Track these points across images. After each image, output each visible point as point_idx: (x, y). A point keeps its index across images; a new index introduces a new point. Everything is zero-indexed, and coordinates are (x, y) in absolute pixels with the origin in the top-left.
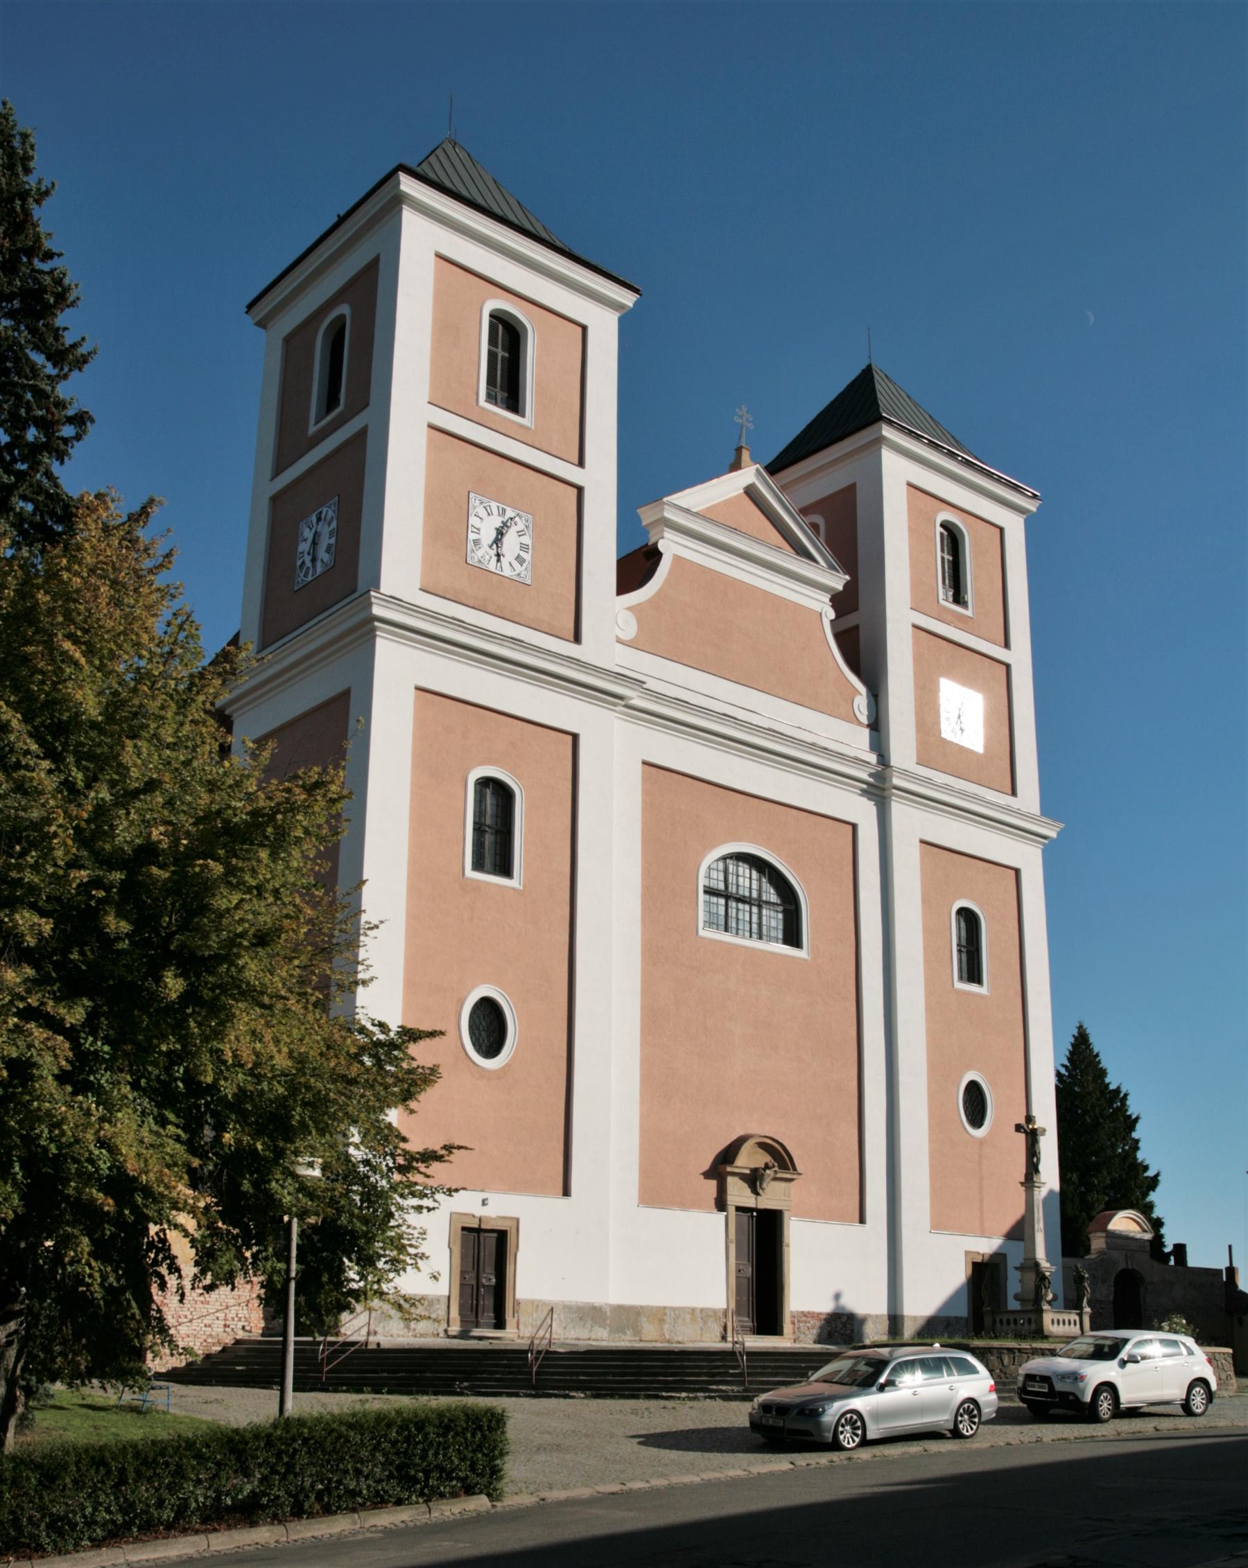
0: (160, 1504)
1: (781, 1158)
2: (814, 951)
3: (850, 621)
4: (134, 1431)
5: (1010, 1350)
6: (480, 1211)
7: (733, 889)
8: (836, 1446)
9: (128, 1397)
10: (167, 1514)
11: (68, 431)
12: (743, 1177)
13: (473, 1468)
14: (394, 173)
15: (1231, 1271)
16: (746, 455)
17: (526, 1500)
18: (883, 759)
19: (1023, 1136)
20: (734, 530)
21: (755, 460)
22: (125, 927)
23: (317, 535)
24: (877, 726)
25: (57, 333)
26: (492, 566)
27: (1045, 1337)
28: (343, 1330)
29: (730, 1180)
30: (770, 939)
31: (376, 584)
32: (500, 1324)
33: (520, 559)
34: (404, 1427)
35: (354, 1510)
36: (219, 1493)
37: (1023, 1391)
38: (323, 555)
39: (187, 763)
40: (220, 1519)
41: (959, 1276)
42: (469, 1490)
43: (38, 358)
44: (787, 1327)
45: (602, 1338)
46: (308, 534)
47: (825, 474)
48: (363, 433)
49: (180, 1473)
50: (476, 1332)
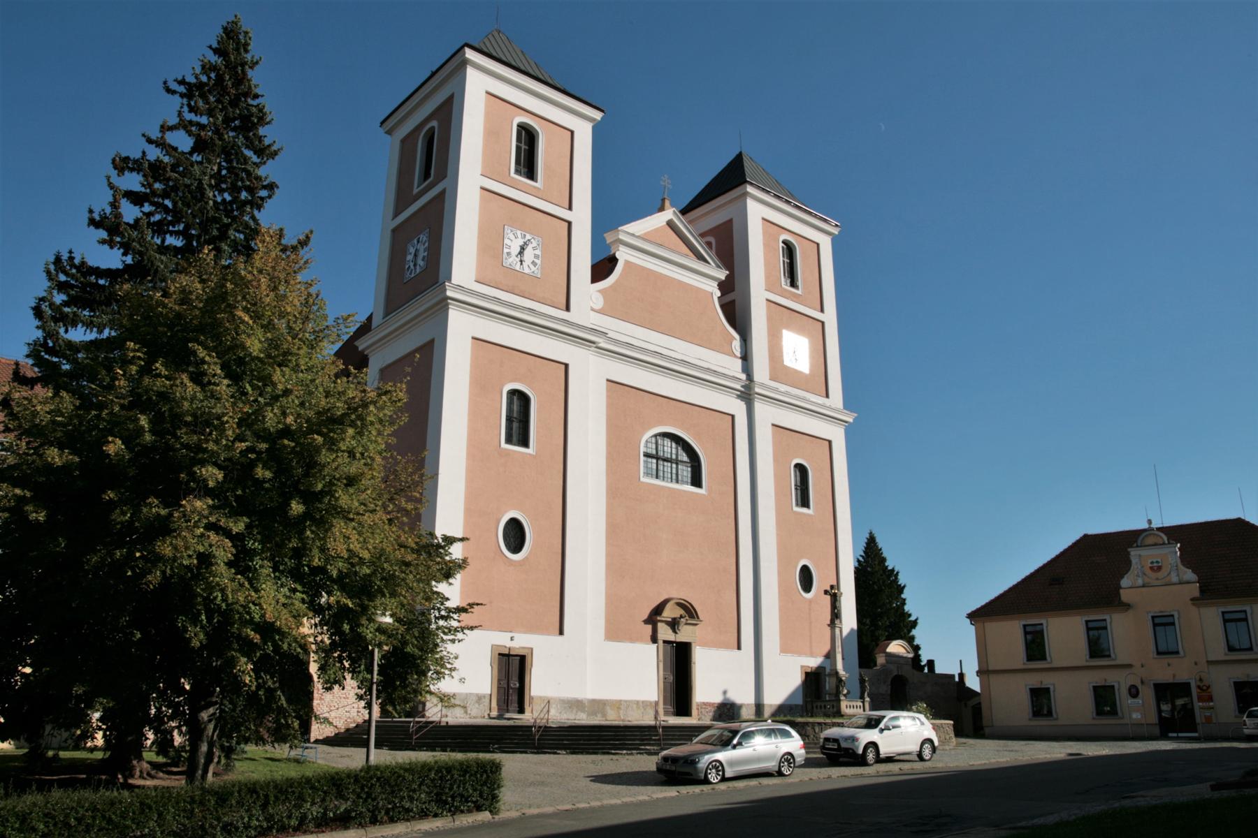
0: (289, 817)
1: (690, 612)
2: (709, 490)
3: (729, 298)
4: (293, 772)
5: (819, 724)
6: (509, 644)
7: (661, 454)
8: (706, 781)
9: (293, 753)
10: (294, 822)
11: (263, 193)
12: (667, 623)
13: (481, 796)
14: (462, 47)
15: (961, 675)
16: (667, 203)
17: (514, 814)
18: (750, 377)
19: (828, 597)
20: (660, 245)
21: (672, 206)
22: (268, 474)
23: (418, 249)
24: (746, 358)
25: (260, 139)
26: (518, 267)
27: (842, 716)
28: (427, 714)
29: (660, 625)
30: (683, 482)
31: (449, 279)
32: (521, 711)
33: (534, 263)
34: (439, 771)
35: (408, 820)
36: (326, 809)
37: (823, 748)
38: (420, 262)
39: (313, 381)
40: (327, 825)
41: (796, 680)
42: (479, 808)
43: (249, 153)
44: (694, 711)
45: (583, 719)
46: (412, 250)
47: (713, 214)
48: (443, 193)
49: (301, 798)
50: (507, 715)
